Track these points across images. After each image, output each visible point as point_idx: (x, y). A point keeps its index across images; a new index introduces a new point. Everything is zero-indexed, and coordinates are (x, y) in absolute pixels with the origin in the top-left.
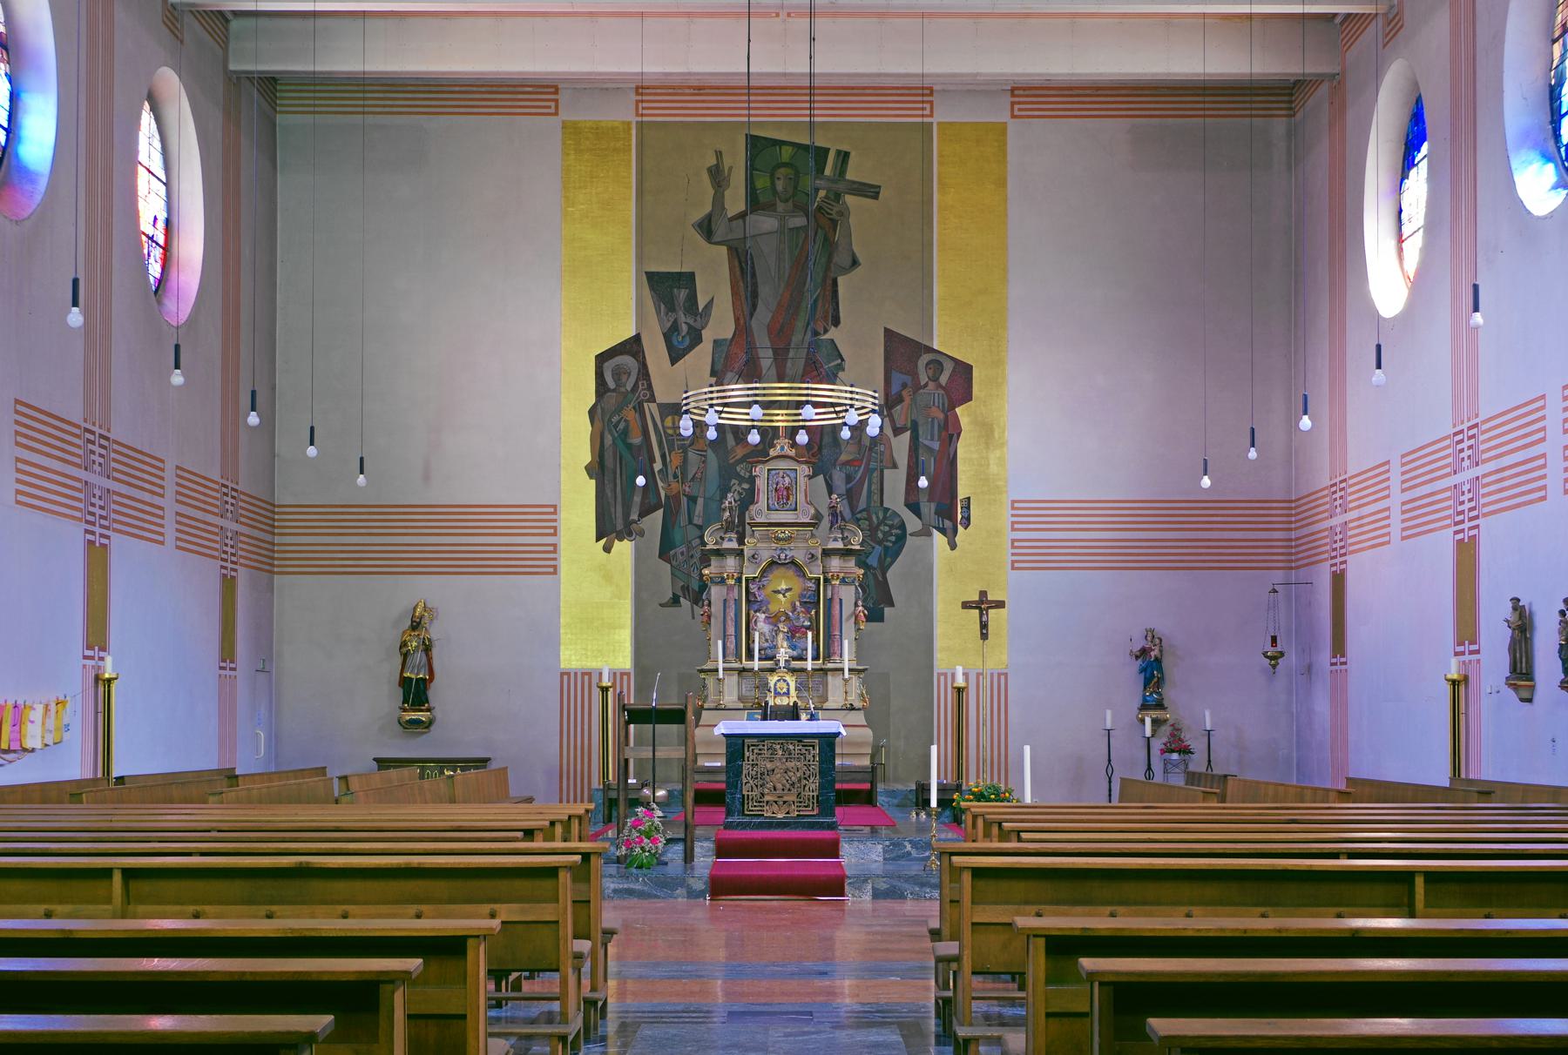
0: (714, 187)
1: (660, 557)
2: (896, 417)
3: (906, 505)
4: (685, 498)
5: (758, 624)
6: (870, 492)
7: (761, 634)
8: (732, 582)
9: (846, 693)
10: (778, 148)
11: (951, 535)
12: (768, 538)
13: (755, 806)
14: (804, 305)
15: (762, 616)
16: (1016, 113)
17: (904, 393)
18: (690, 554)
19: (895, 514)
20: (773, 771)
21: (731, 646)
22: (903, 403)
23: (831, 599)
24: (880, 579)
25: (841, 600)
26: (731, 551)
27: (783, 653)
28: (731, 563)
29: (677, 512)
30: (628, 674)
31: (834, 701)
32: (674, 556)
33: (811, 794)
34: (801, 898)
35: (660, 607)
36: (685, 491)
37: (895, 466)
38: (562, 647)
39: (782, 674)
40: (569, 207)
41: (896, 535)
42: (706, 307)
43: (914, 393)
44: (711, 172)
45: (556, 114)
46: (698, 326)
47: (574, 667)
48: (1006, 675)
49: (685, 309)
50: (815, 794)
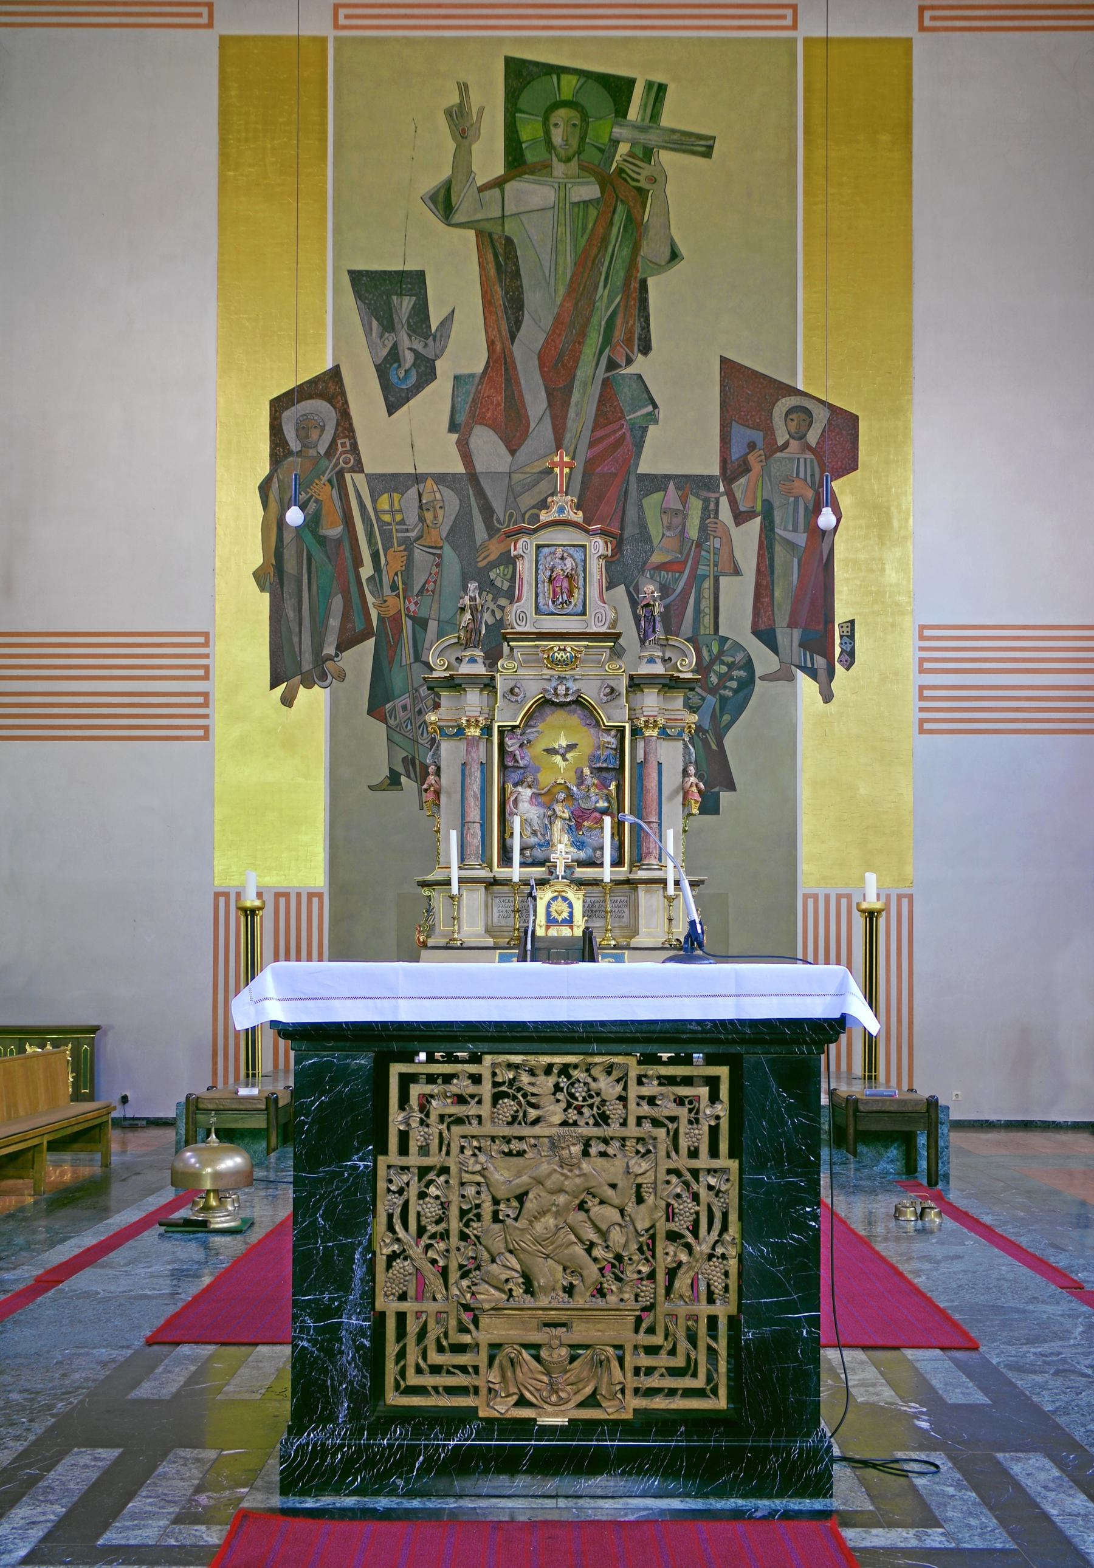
0: (454, 138)
1: (370, 712)
2: (738, 495)
4: (410, 623)
5: (520, 805)
6: (698, 611)
7: (525, 822)
8: (475, 732)
9: (670, 920)
10: (555, 77)
11: (825, 678)
12: (537, 661)
13: (436, 1370)
14: (594, 321)
15: (526, 793)
16: (927, 23)
19: (738, 647)
20: (521, 1198)
21: (474, 840)
23: (643, 764)
24: (714, 747)
25: (660, 764)
26: (473, 679)
27: (562, 852)
28: (473, 698)
30: (320, 895)
31: (649, 935)
33: (704, 1309)
36: (408, 609)
37: (737, 572)
38: (217, 854)
40: (229, 170)
41: (738, 679)
42: (442, 324)
44: (451, 116)
45: (210, 25)
46: (429, 353)
47: (234, 883)
48: (910, 897)
50: (722, 1310)
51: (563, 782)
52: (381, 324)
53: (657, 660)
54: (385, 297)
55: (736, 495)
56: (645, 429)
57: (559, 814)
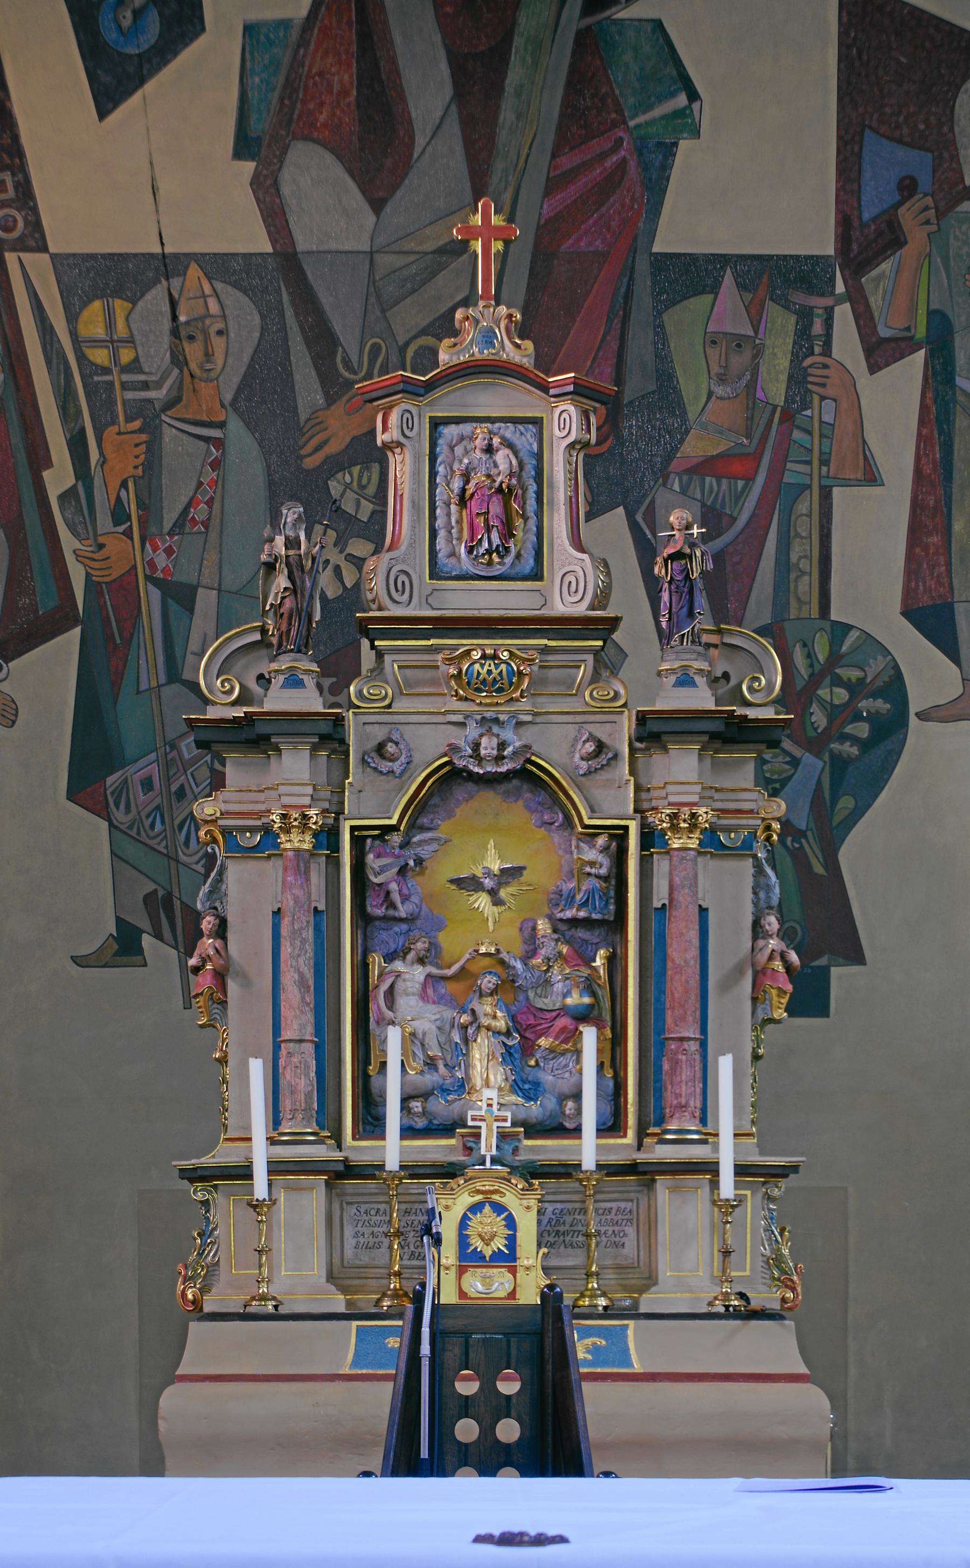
1: (72, 796)
2: (876, 301)
3: (906, 614)
4: (155, 594)
6: (783, 565)
7: (411, 1039)
8: (297, 841)
9: (726, 1253)
17: (906, 215)
18: (174, 788)
24: (819, 869)
29: (128, 642)
32: (118, 794)
34: (480, 1302)
35: (75, 970)
36: (152, 564)
37: (871, 477)
41: (873, 719)
43: (940, 215)
55: (872, 300)
56: (669, 150)
57: (485, 1021)
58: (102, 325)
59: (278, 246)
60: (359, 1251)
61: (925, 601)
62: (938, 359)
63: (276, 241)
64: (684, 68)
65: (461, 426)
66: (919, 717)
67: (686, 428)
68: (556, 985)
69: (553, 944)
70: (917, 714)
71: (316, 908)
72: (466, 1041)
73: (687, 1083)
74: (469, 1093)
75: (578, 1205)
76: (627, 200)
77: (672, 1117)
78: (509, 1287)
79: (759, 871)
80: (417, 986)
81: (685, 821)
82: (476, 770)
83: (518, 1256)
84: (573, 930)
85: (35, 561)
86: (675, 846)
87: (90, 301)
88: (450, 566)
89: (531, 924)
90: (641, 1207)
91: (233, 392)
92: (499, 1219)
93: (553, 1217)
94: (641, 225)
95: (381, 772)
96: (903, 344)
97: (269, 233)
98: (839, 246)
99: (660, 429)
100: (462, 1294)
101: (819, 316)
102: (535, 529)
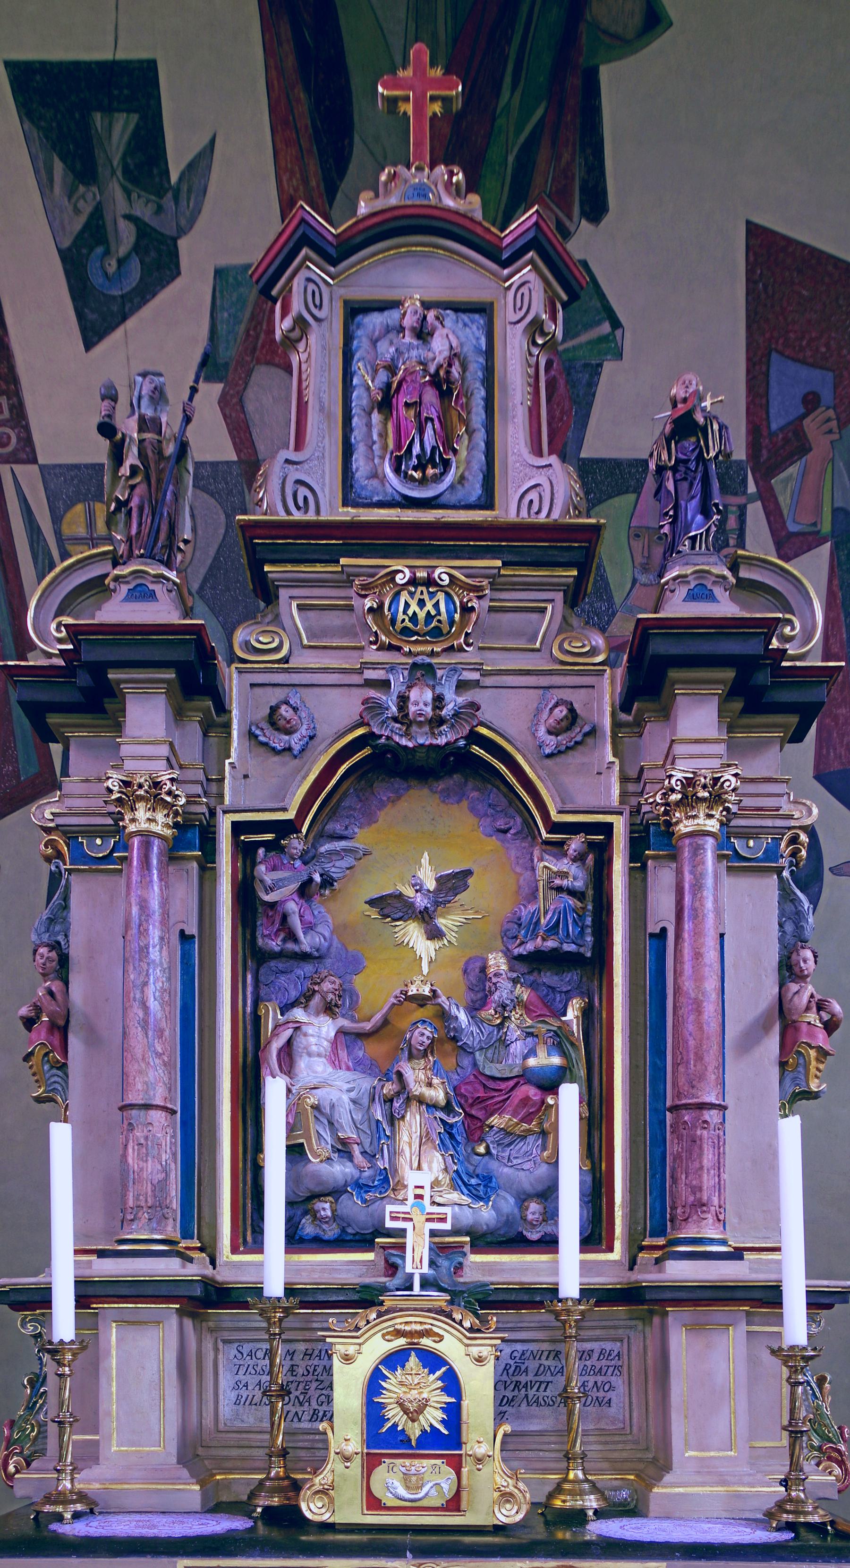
2: (784, 500)
5: (302, 1064)
22: (809, 457)
39: (414, 1323)
42: (191, 166)
49: (126, 171)
51: (426, 990)
52: (70, 168)
53: (718, 591)
54: (77, 115)
55: (781, 499)
56: (596, 370)
57: (417, 1089)
58: (83, 525)
59: (242, 455)
60: (240, 1407)
61: (836, 766)
62: (843, 550)
63: (241, 451)
64: (608, 301)
65: (386, 313)
66: (832, 872)
67: (613, 611)
68: (513, 1045)
69: (510, 985)
70: (830, 869)
71: (182, 932)
72: (392, 1120)
73: (708, 1170)
74: (394, 1190)
75: (546, 1346)
76: (557, 413)
77: (686, 1220)
78: (448, 1487)
79: (786, 895)
80: (325, 1044)
81: (704, 787)
82: (404, 742)
83: (464, 1439)
84: (535, 974)
85: (18, 732)
86: (685, 830)
87: (73, 505)
88: (370, 488)
89: (478, 964)
90: (634, 1349)
91: (200, 582)
92: (432, 1377)
93: (512, 1362)
94: (570, 434)
95: (274, 749)
96: (810, 538)
97: (234, 444)
98: (750, 452)
99: (589, 612)
100: (374, 1503)
101: (733, 513)
102: (483, 444)
